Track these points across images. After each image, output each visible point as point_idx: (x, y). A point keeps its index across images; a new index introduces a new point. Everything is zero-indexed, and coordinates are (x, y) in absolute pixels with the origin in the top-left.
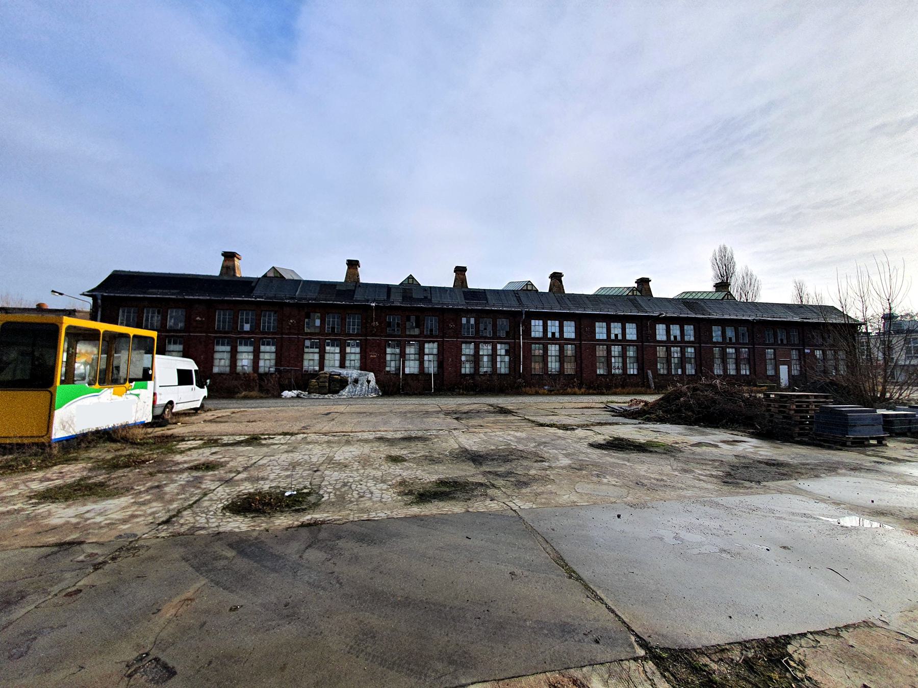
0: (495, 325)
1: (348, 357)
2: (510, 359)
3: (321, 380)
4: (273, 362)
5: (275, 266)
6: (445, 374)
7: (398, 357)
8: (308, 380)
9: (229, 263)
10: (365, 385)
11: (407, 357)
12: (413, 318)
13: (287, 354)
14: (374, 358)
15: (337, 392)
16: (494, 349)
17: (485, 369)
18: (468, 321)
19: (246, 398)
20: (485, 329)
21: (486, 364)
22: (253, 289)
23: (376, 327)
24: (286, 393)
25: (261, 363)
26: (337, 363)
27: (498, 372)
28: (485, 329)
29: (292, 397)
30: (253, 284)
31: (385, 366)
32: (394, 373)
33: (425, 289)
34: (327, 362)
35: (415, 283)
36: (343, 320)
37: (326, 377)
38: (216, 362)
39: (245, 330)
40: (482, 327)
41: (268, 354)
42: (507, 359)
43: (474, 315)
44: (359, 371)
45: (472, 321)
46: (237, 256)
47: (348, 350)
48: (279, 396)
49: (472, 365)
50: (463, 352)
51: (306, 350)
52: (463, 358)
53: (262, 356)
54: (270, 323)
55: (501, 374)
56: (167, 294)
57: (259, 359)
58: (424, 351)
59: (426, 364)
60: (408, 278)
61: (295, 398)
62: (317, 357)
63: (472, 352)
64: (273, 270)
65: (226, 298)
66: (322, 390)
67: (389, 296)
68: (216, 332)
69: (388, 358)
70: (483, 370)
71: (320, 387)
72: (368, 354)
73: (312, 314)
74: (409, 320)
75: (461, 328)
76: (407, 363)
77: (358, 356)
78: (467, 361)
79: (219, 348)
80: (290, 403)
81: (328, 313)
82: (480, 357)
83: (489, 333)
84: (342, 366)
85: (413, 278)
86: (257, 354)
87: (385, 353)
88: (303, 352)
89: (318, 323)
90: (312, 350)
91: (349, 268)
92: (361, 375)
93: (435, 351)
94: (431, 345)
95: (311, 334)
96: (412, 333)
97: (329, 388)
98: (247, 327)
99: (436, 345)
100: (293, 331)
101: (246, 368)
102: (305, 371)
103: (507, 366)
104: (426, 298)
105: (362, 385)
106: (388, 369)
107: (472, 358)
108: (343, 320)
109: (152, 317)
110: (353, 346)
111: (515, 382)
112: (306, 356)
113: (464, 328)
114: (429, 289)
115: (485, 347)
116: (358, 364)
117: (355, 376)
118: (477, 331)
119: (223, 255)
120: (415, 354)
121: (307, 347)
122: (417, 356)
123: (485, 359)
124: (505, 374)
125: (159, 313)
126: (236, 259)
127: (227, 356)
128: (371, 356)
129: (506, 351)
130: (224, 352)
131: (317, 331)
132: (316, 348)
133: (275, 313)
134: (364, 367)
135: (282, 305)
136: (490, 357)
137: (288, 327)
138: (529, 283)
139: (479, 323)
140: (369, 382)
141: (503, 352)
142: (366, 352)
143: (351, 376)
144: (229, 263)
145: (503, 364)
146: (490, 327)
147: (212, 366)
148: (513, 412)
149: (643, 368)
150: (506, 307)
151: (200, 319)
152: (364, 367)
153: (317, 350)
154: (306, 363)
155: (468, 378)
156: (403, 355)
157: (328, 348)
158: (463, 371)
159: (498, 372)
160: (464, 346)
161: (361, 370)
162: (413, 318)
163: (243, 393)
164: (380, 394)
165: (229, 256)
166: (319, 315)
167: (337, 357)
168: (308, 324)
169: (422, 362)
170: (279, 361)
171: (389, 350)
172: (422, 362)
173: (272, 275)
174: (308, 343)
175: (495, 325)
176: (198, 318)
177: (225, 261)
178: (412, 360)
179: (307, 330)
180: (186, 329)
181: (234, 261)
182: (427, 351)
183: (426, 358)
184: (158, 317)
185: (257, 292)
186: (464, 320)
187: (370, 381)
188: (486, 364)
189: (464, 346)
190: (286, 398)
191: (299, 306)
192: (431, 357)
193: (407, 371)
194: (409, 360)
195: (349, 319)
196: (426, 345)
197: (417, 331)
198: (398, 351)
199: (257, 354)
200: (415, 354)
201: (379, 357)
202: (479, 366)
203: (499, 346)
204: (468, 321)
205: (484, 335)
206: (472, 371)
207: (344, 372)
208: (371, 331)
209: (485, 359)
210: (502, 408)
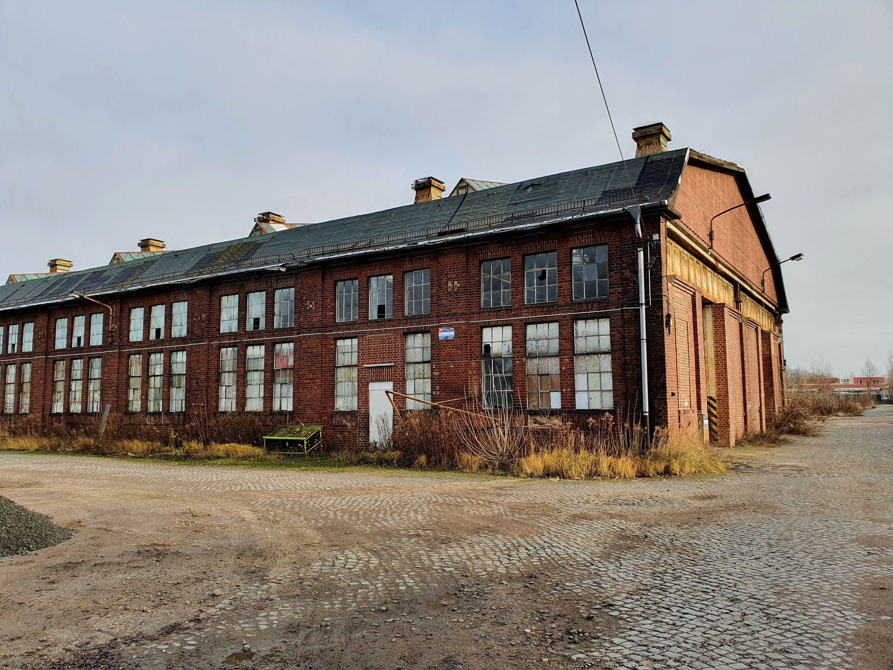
80: (538, 484)
94: (542, 329)
196: (531, 330)
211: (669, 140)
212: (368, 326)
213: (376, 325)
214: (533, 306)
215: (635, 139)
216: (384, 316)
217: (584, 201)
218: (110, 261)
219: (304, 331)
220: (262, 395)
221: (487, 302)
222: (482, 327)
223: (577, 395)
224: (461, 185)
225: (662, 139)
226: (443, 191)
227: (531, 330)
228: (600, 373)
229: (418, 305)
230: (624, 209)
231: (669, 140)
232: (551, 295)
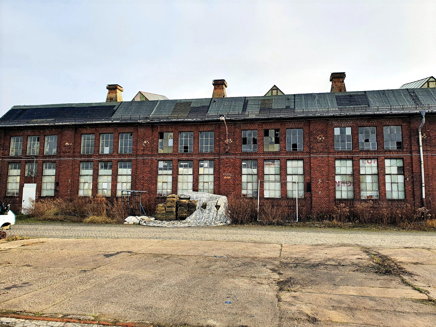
0: (380, 136)
1: (201, 179)
2: (405, 179)
3: (168, 204)
4: (129, 185)
5: (140, 91)
6: (314, 199)
7: (255, 177)
8: (156, 204)
9: (113, 95)
10: (213, 211)
11: (266, 178)
12: (272, 132)
13: (141, 176)
14: (228, 180)
15: (184, 218)
16: (381, 167)
17: (369, 194)
18: (343, 132)
19: (93, 223)
20: (367, 141)
21: (369, 187)
22: (114, 112)
23: (230, 144)
24: (131, 219)
25: (119, 186)
26: (190, 186)
27: (388, 196)
28: (367, 141)
29: (134, 223)
30: (115, 109)
31: (241, 189)
32: (251, 196)
33: (288, 98)
34: (180, 185)
35: (279, 94)
36: (196, 138)
37: (174, 201)
38: (81, 186)
39: (105, 153)
40: (361, 138)
41: (125, 176)
42: (401, 179)
43: (351, 123)
44: (211, 195)
45: (348, 131)
46: (118, 87)
47: (201, 171)
48: (121, 222)
49: (351, 188)
50: (338, 171)
51: (160, 172)
52: (338, 179)
53: (119, 178)
54: (126, 145)
55: (393, 200)
56: (44, 122)
57: (117, 182)
58: (286, 171)
59: (289, 187)
60: (272, 89)
61: (136, 224)
62: (170, 179)
63: (349, 171)
64: (139, 94)
65: (87, 123)
66: (167, 217)
67: (244, 108)
68: (81, 156)
69: (244, 178)
70: (364, 195)
71: (167, 212)
72: (221, 176)
73: (165, 134)
74: (266, 134)
75: (333, 141)
76: (266, 185)
77: (211, 178)
78: (343, 183)
79: (83, 172)
80: (132, 229)
81: (181, 132)
82: (361, 177)
83: (372, 146)
84: (195, 189)
85: (278, 89)
86: (115, 176)
87: (241, 174)
88: (157, 174)
89: (171, 142)
90: (165, 172)
91: (215, 89)
92: (211, 199)
93: (301, 171)
94: (295, 163)
95: (163, 155)
96: (271, 150)
97: (177, 214)
98: (107, 150)
99: (301, 163)
100: (146, 152)
101: (105, 191)
102: (159, 194)
103: (401, 188)
104: (288, 107)
105: (210, 210)
106: (244, 192)
107: (350, 179)
108: (196, 138)
109: (34, 144)
110: (185, 166)
111: (415, 212)
112: (160, 178)
113: (338, 141)
114: (293, 98)
115: (367, 164)
116: (211, 187)
117: (204, 200)
118: (355, 143)
119: (107, 88)
120: (275, 175)
121: (161, 169)
122: (278, 177)
123: (369, 179)
124: (398, 200)
125: (38, 141)
126: (118, 90)
127: (89, 179)
128: (225, 177)
129: (399, 168)
130: (88, 175)
131: (171, 151)
132: (170, 169)
133: (131, 135)
134: (217, 191)
135: (135, 125)
136: (376, 177)
137: (142, 148)
138: (432, 79)
139: (357, 134)
140: (218, 207)
141: (394, 170)
142: (219, 172)
143: (200, 201)
144: (113, 95)
145: (395, 186)
146: (373, 138)
147: (78, 190)
148: (405, 272)
149: (49, 162)
150: (395, 109)
151: (68, 144)
152: (217, 191)
153: (170, 172)
154: (159, 185)
155: (343, 205)
156: (261, 175)
157: (181, 169)
158: (338, 196)
159: (388, 196)
160: (338, 163)
161: (214, 193)
162: (272, 132)
163: (91, 218)
164: (229, 222)
165: (113, 88)
166: (172, 134)
167: (191, 178)
168: (162, 143)
169: (284, 185)
170: (134, 185)
171: (244, 171)
172: (284, 185)
173: (138, 99)
174: (161, 164)
175: (380, 136)
176: (67, 144)
177: (109, 93)
178: (272, 182)
179: (161, 151)
180: (59, 154)
181: (116, 92)
182: (289, 171)
183: (289, 178)
184: (37, 144)
185: (117, 115)
186: (337, 131)
187: (219, 206)
188: (369, 187)
189: (338, 163)
190: (129, 225)
191: (152, 125)
192: (295, 178)
193: (267, 195)
194: (269, 181)
195: (202, 137)
196: (289, 163)
197: (276, 148)
198: (255, 171)
199: (115, 176)
200: (275, 175)
201: (234, 179)
202: (359, 188)
203: (387, 162)
204: (343, 132)
205: (366, 148)
206: (351, 195)
207: (194, 195)
208: (225, 149)
209: (369, 179)
210: (384, 258)
211: (226, 87)
212: (51, 158)
213: (86, 157)
214: (395, 151)
215: (213, 84)
216: (297, 150)
217: (403, 105)
218: (300, 93)
219: (95, 157)
220: (91, 188)
221: (84, 152)
222: (158, 161)
223: (337, 192)
224: (273, 88)
225: (224, 86)
226: (122, 91)
227: (289, 163)
228: (372, 183)
229: (126, 149)
230: (429, 111)
231: (226, 87)
232: (93, 151)
